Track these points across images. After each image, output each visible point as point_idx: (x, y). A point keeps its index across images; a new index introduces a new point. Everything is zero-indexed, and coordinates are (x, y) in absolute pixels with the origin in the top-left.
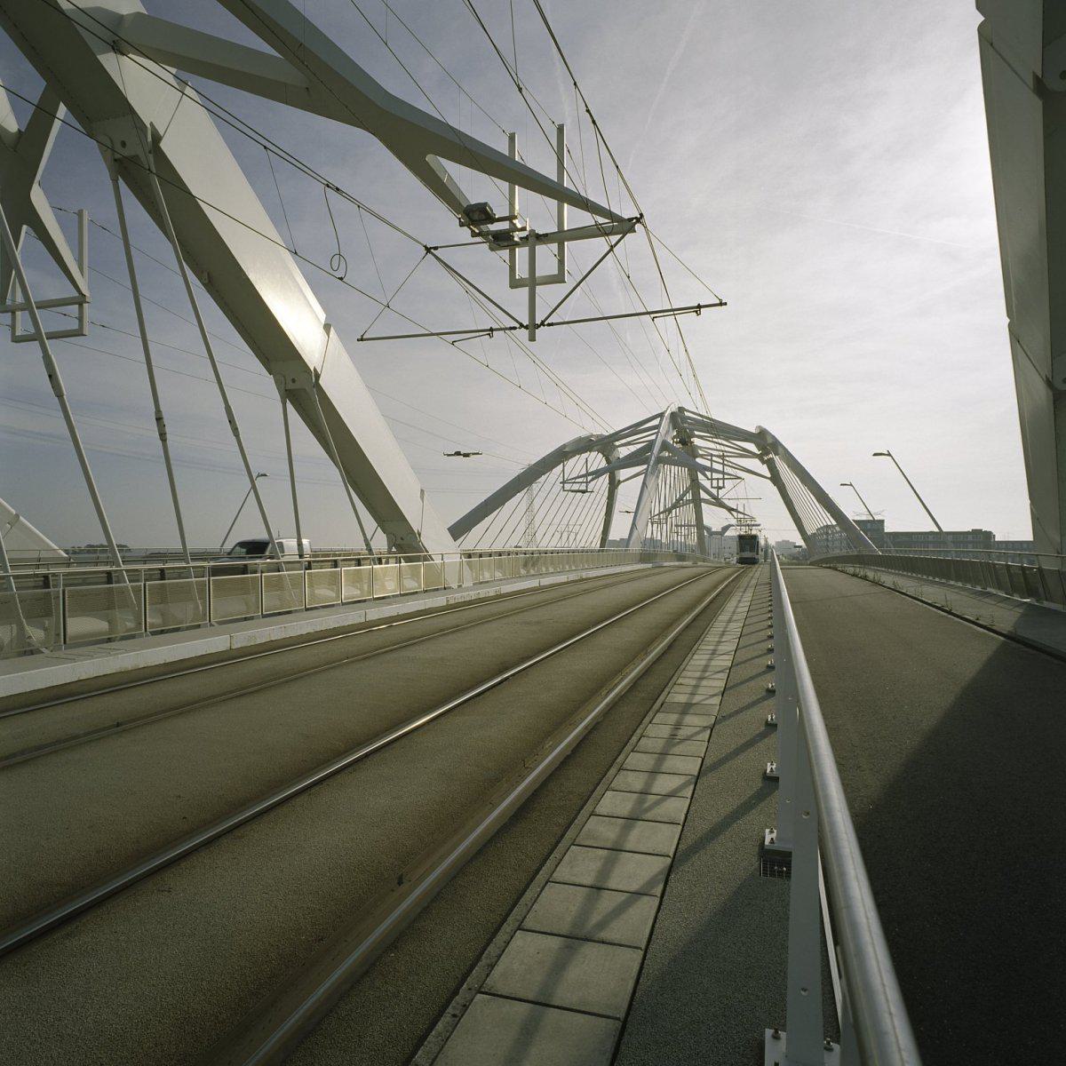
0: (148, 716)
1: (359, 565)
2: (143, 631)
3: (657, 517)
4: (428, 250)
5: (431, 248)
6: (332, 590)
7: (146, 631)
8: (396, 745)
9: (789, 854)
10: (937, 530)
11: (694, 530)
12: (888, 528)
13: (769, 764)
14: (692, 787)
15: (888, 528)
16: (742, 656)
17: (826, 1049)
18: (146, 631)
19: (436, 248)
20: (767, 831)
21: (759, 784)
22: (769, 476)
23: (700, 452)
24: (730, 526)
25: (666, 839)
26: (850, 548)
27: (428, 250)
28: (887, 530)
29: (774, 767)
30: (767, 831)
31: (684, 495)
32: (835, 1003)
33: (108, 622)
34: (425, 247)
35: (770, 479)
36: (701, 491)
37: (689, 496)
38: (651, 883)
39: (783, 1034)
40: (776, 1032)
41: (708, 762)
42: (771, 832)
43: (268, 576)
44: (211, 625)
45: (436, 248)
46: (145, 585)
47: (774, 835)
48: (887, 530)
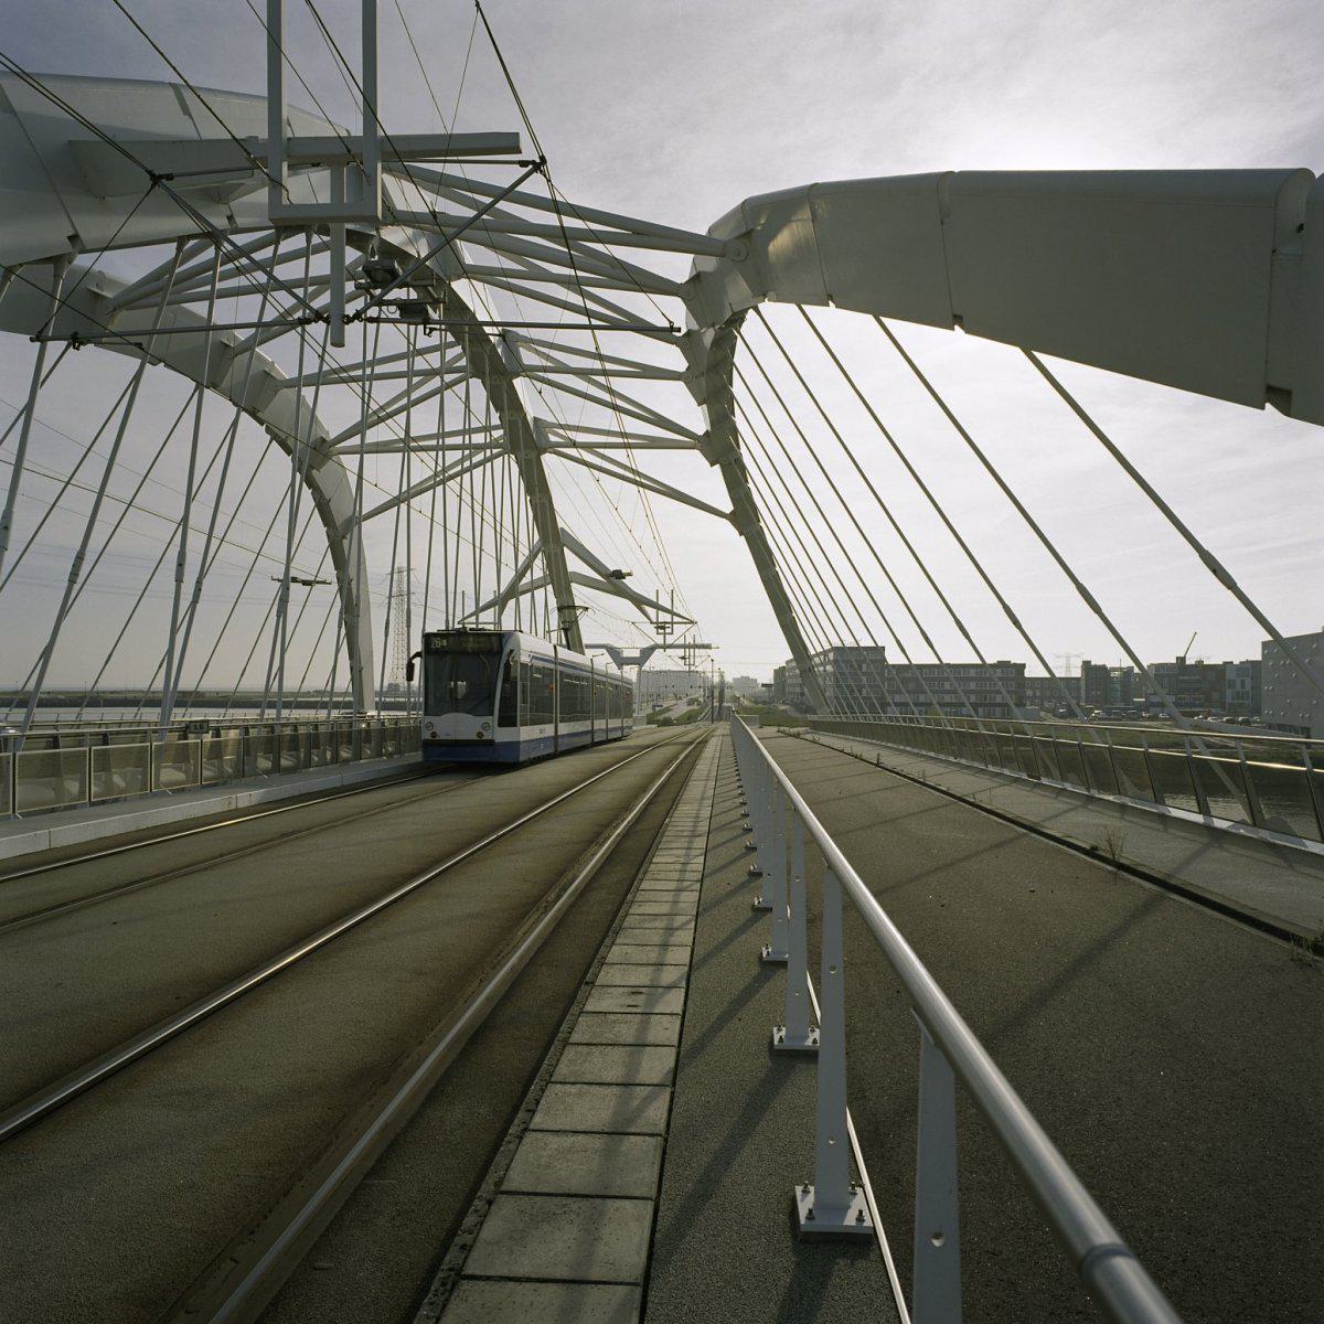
0: (327, 829)
1: (106, 743)
2: (11, 812)
3: (473, 619)
4: (156, 179)
5: (161, 177)
6: (179, 769)
7: (14, 812)
8: (526, 824)
9: (518, 133)
10: (1048, 676)
11: (313, 578)
12: (1093, 663)
13: (764, 949)
14: (694, 923)
15: (1093, 663)
16: (717, 838)
17: (851, 1193)
18: (14, 812)
19: (170, 177)
20: (775, 1029)
21: (755, 970)
22: (728, 507)
23: (553, 438)
24: (652, 649)
25: (682, 956)
26: (838, 713)
27: (156, 179)
28: (1027, 674)
29: (770, 950)
30: (775, 1029)
31: (528, 566)
32: (529, 234)
33: (53, 789)
34: (150, 172)
35: (732, 518)
36: (565, 548)
37: (538, 570)
38: (680, 980)
39: (812, 1189)
40: (806, 1186)
41: (700, 951)
42: (779, 1030)
43: (25, 756)
44: (16, 817)
45: (170, 177)
46: (14, 754)
47: (783, 1033)
48: (1027, 674)
